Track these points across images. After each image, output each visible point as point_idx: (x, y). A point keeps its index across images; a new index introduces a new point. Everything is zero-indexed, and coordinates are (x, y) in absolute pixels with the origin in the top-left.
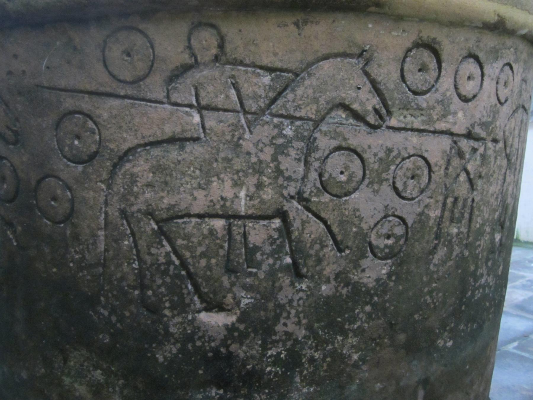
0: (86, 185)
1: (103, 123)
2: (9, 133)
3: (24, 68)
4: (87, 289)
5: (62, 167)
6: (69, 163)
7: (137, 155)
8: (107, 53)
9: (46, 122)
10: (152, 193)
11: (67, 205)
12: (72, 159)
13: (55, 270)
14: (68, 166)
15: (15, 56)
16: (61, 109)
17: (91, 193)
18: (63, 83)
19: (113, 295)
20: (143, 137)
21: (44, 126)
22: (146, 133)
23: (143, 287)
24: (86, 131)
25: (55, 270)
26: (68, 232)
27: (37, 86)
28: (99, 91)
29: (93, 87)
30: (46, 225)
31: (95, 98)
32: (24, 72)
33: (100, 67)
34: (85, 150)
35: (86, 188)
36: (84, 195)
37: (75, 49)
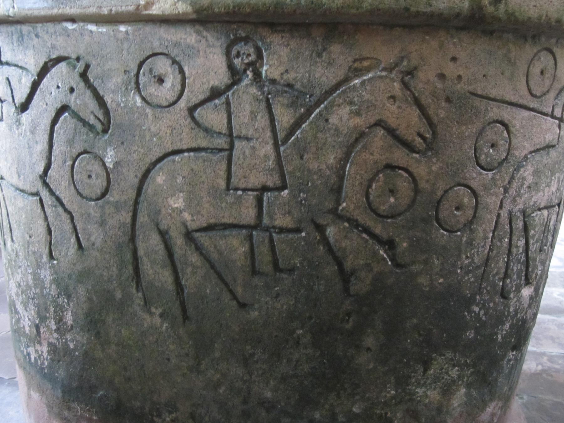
0: (492, 191)
1: (514, 132)
2: (419, 140)
3: (461, 73)
4: (468, 292)
5: (474, 175)
6: (482, 171)
7: (528, 161)
8: (531, 68)
9: (469, 130)
10: (173, 198)
11: (470, 212)
12: (485, 167)
13: (441, 280)
14: (481, 174)
15: (454, 59)
16: (487, 118)
17: (494, 198)
18: (493, 93)
19: (487, 291)
20: (534, 145)
21: (467, 134)
22: (536, 140)
23: (504, 279)
24: (502, 140)
25: (441, 280)
26: (464, 239)
27: (471, 93)
28: (519, 103)
29: (514, 99)
30: (443, 235)
31: (514, 109)
32: (459, 77)
33: (524, 80)
34: (497, 157)
35: (491, 194)
36: (488, 200)
37: (510, 61)
